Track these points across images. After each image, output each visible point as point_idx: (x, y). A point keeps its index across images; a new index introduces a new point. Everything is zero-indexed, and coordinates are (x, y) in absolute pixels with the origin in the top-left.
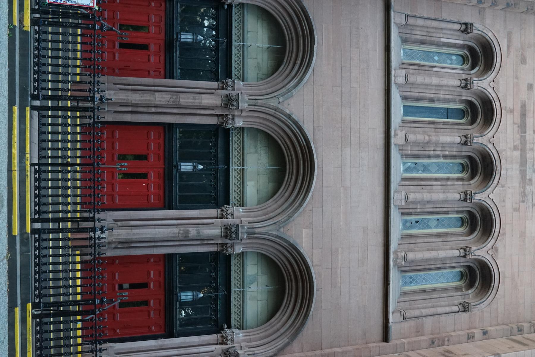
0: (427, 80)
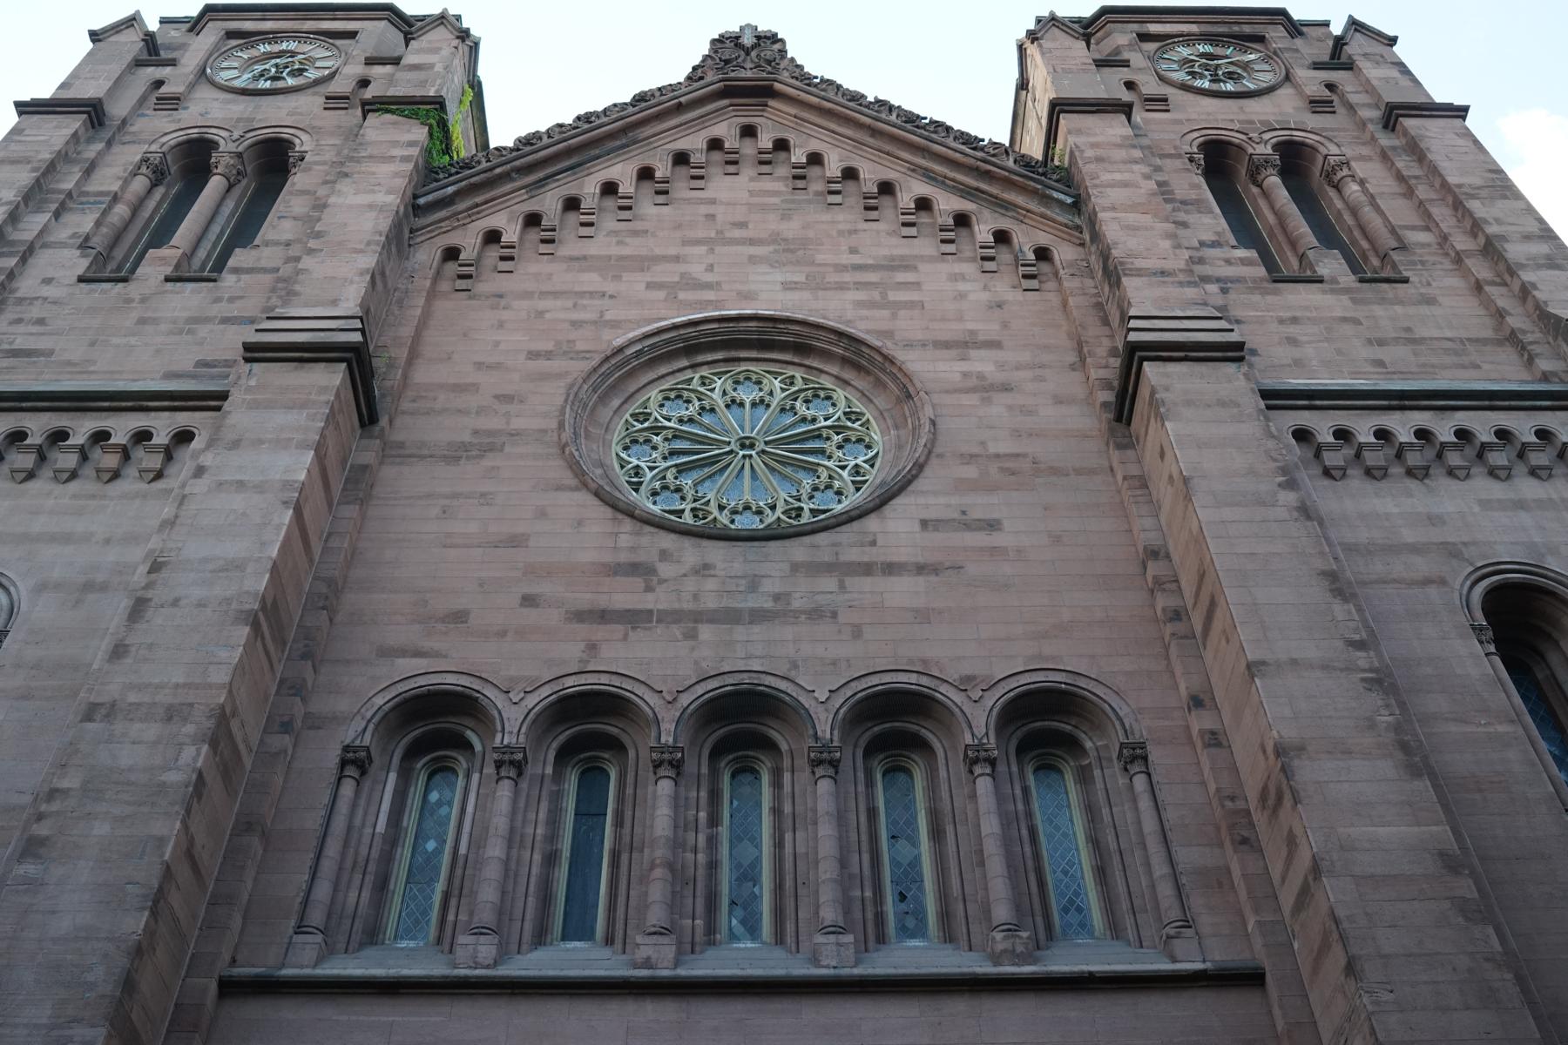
0: (492, 872)
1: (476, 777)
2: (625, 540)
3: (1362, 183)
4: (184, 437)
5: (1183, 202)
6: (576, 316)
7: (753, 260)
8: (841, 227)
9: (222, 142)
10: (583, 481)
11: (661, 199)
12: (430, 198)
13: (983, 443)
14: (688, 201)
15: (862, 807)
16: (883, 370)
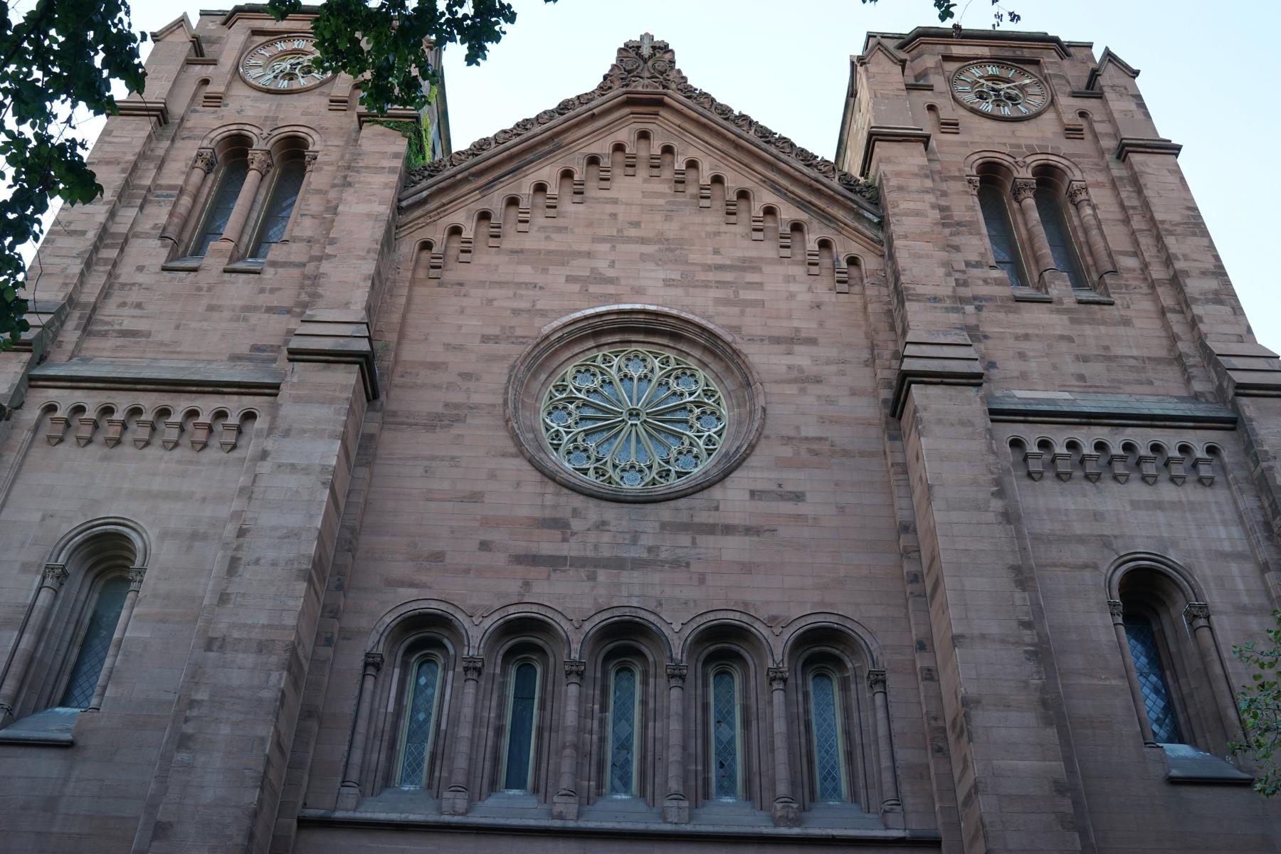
0: (463, 747)
1: (451, 673)
2: (549, 500)
3: (1094, 208)
4: (249, 416)
5: (959, 224)
6: (516, 305)
7: (644, 257)
8: (709, 229)
9: (255, 139)
10: (521, 451)
11: (578, 198)
12: (410, 201)
13: (797, 428)
14: (597, 200)
15: (699, 705)
16: (732, 360)
